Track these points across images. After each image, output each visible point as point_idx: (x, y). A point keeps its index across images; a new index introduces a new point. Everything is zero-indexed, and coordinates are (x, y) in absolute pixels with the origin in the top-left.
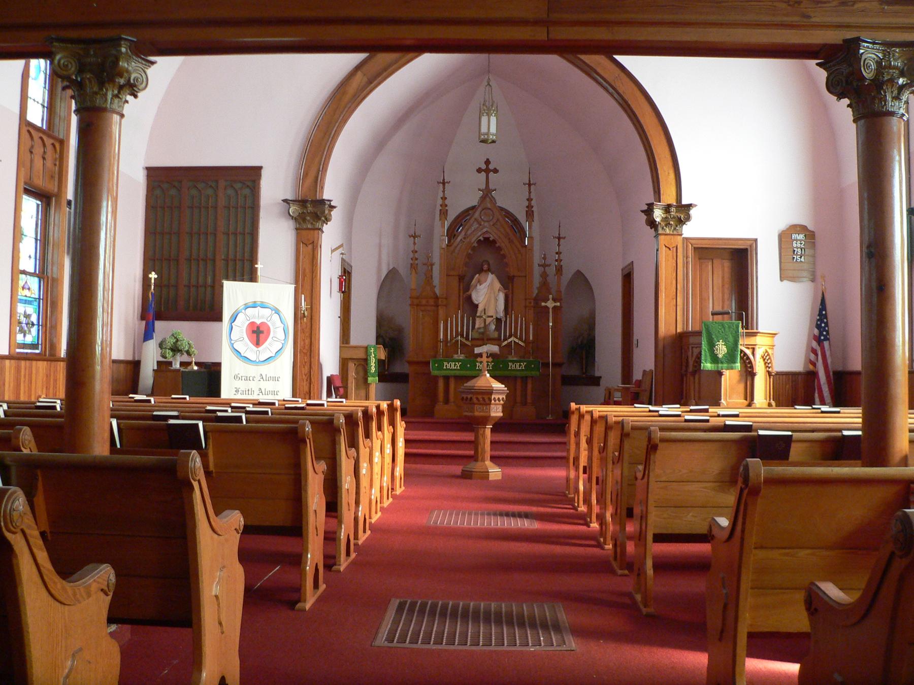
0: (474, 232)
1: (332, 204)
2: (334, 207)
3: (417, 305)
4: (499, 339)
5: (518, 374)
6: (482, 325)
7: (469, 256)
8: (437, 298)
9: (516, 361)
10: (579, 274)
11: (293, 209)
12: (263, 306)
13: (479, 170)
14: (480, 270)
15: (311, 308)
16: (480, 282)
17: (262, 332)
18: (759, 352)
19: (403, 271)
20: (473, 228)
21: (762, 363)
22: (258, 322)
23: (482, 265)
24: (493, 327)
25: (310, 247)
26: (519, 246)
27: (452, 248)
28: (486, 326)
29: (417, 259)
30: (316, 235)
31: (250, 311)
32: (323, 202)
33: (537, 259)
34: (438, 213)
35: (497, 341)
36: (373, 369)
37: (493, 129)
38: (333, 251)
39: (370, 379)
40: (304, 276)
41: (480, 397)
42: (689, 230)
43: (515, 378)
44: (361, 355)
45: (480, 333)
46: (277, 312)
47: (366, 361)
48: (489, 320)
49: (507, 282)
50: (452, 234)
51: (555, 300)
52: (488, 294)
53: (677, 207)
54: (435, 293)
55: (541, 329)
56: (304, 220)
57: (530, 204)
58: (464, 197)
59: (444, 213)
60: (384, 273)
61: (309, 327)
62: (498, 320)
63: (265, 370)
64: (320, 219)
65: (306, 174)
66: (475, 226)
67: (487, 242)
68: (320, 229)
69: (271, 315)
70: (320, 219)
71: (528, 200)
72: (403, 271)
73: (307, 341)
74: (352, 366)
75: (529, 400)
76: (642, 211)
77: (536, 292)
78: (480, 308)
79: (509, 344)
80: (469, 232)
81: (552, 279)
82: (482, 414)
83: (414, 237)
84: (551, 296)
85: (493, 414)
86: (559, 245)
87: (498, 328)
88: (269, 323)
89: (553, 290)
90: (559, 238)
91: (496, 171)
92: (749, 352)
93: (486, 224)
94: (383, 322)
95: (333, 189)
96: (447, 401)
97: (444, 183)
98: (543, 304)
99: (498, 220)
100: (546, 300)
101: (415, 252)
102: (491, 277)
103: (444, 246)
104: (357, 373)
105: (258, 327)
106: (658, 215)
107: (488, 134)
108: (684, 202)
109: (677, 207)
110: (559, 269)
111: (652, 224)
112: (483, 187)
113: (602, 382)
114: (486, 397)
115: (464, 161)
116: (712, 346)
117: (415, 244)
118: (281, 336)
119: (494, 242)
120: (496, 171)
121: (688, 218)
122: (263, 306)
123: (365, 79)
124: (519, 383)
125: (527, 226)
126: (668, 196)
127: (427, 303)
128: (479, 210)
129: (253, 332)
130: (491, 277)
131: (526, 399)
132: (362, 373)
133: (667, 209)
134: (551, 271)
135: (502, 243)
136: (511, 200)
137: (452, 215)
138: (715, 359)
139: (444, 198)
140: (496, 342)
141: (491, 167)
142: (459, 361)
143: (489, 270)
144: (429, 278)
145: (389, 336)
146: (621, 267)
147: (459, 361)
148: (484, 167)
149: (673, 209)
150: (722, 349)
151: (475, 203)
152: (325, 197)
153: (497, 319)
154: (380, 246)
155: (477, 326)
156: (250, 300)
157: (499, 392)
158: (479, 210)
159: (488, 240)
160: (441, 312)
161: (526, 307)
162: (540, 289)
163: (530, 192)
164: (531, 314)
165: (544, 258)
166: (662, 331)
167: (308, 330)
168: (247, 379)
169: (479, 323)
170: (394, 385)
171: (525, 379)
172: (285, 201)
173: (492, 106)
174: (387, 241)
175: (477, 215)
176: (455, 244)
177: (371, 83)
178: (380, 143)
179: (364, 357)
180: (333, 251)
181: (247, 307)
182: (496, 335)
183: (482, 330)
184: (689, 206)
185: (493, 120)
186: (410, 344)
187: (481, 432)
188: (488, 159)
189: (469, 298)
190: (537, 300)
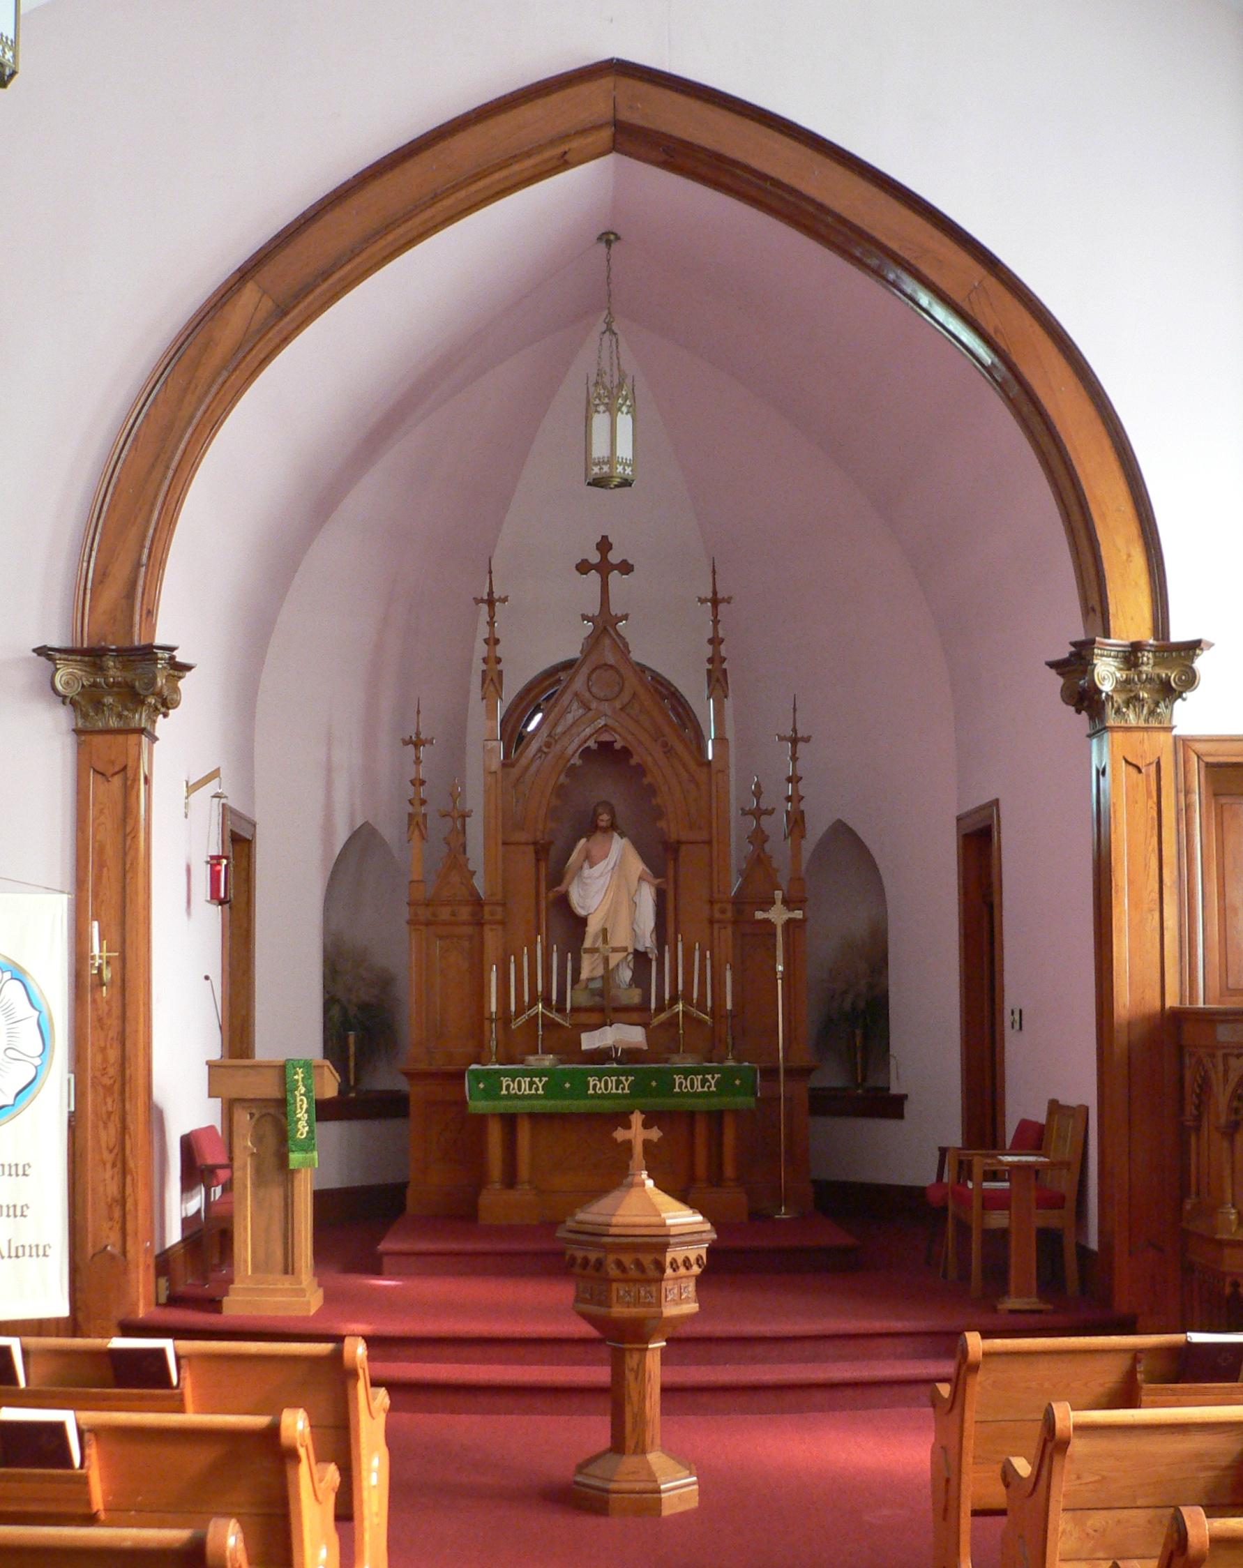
0: (572, 727)
1: (180, 657)
2: (188, 668)
3: (428, 924)
4: (643, 1007)
5: (701, 1104)
6: (600, 971)
7: (560, 791)
8: (478, 903)
9: (695, 1072)
10: (842, 833)
13: (583, 567)
14: (590, 827)
15: (123, 958)
16: (590, 859)
19: (390, 831)
20: (570, 718)
23: (595, 815)
24: (626, 975)
25: (117, 781)
26: (692, 766)
27: (515, 772)
28: (608, 975)
29: (423, 802)
30: (132, 751)
32: (148, 653)
33: (736, 796)
34: (476, 680)
35: (637, 1013)
37: (625, 449)
38: (192, 788)
39: (295, 1158)
40: (101, 865)
41: (627, 1259)
43: (691, 1115)
44: (270, 1090)
45: (594, 993)
47: (282, 1105)
48: (615, 959)
49: (662, 857)
50: (514, 736)
51: (788, 903)
52: (612, 891)
53: (1157, 650)
54: (473, 892)
55: (754, 985)
56: (98, 705)
57: (716, 651)
58: (546, 635)
59: (492, 680)
60: (342, 836)
61: (116, 1011)
62: (640, 958)
64: (142, 703)
65: (102, 576)
66: (576, 711)
67: (607, 754)
68: (142, 731)
70: (142, 703)
71: (711, 641)
72: (390, 831)
73: (113, 1054)
74: (243, 1118)
75: (729, 1171)
76: (1052, 665)
78: (593, 927)
79: (672, 1022)
80: (559, 730)
81: (779, 849)
82: (634, 1311)
83: (417, 743)
84: (778, 895)
85: (670, 1311)
86: (794, 758)
87: (640, 978)
89: (783, 879)
90: (795, 741)
91: (625, 568)
93: (605, 707)
94: (338, 963)
95: (189, 611)
96: (510, 1180)
97: (491, 602)
98: (759, 915)
99: (634, 695)
100: (768, 903)
101: (418, 782)
102: (619, 846)
103: (495, 765)
104: (258, 1140)
106: (1106, 673)
107: (611, 460)
108: (1178, 634)
109: (1157, 650)
110: (797, 822)
111: (1086, 700)
112: (594, 610)
113: (908, 1108)
114: (647, 1259)
115: (545, 531)
117: (418, 761)
118: (33, 1044)
119: (626, 752)
120: (625, 568)
121: (1190, 680)
123: (267, 304)
124: (701, 1128)
125: (707, 712)
126: (1130, 620)
127: (455, 915)
128: (585, 670)
130: (619, 846)
131: (720, 1166)
132: (271, 1141)
133: (1131, 656)
134: (776, 825)
135: (647, 753)
136: (667, 646)
137: (513, 685)
139: (493, 641)
140: (635, 1016)
141: (614, 557)
142: (540, 1073)
143: (613, 827)
145: (357, 1020)
146: (956, 813)
147: (540, 1073)
148: (595, 558)
149: (1147, 657)
151: (574, 652)
152: (159, 640)
153: (637, 953)
154: (329, 770)
155: (584, 975)
157: (688, 1238)
158: (585, 670)
159: (612, 749)
160: (492, 938)
161: (711, 922)
162: (747, 876)
163: (716, 622)
164: (726, 935)
165: (758, 794)
166: (1125, 1000)
167: (113, 1023)
169: (589, 967)
170: (377, 1127)
171: (716, 1117)
172: (42, 651)
173: (620, 386)
174: (347, 757)
175: (579, 683)
176: (524, 761)
177: (285, 313)
178: (319, 502)
179: (278, 1095)
180: (192, 788)
182: (635, 996)
183: (597, 985)
184: (1193, 647)
185: (624, 422)
186: (411, 1028)
187: (631, 1361)
188: (605, 538)
189: (563, 902)
190: (744, 904)
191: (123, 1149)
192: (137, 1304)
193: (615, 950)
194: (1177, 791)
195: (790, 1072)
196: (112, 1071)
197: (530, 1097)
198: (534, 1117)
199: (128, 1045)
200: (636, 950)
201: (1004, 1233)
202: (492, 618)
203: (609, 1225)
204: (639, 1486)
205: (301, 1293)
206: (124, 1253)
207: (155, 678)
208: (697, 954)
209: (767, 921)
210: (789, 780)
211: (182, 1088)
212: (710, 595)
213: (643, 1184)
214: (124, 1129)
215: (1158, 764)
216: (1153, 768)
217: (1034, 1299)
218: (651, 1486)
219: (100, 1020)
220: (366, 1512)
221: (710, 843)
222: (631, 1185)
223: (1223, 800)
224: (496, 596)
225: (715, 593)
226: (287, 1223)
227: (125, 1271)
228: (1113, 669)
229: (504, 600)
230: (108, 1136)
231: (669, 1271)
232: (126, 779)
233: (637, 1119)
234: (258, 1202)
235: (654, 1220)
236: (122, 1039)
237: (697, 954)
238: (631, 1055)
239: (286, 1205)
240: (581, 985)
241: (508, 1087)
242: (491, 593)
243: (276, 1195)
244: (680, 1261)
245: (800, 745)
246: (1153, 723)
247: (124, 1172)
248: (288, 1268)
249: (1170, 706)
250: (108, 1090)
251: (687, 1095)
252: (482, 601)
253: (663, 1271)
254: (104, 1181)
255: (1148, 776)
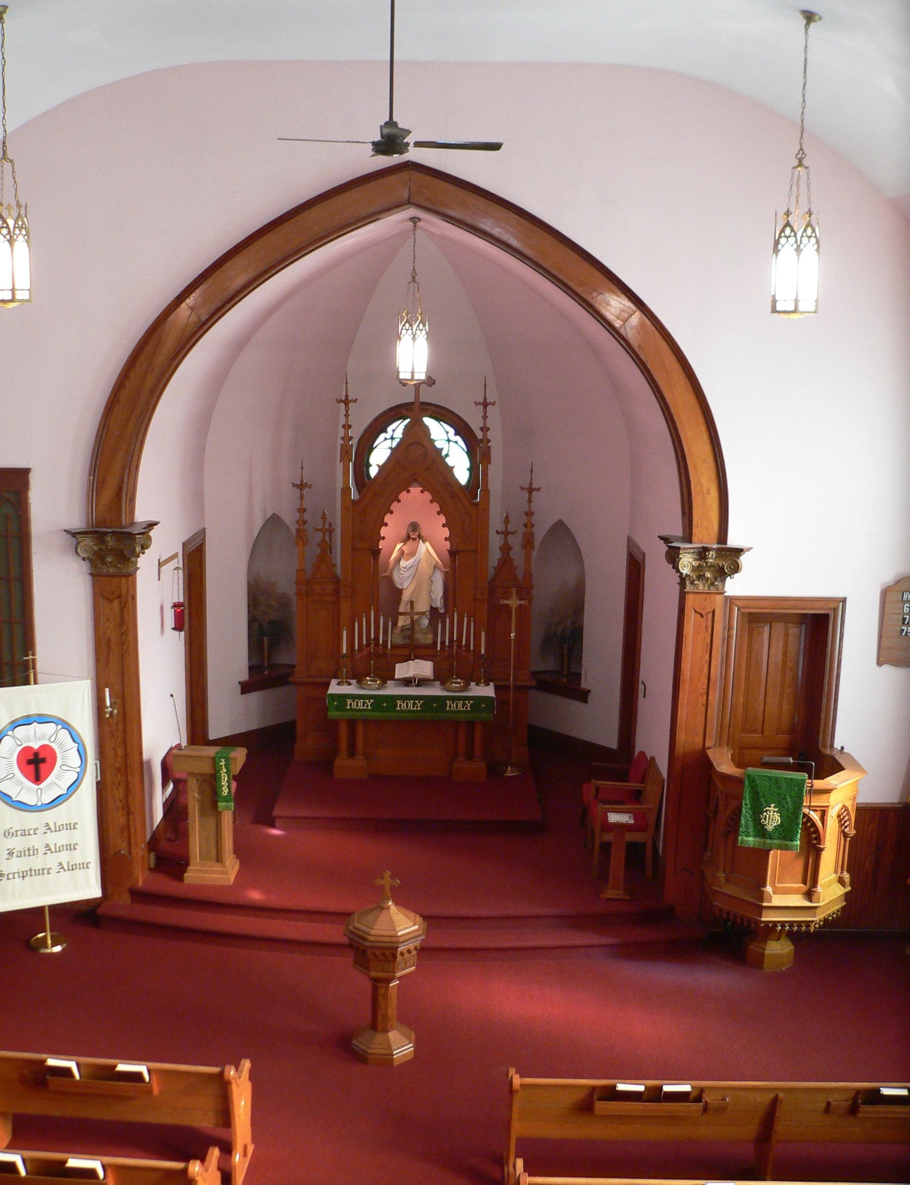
11: (88, 542)
12: (43, 719)
17: (43, 760)
18: (832, 813)
21: (837, 825)
22: (36, 746)
24: (425, 622)
25: (116, 603)
31: (20, 731)
33: (495, 522)
36: (226, 787)
38: (160, 565)
39: (221, 805)
42: (734, 586)
43: (457, 723)
46: (66, 725)
63: (50, 816)
69: (56, 732)
73: (120, 752)
75: (478, 752)
77: (491, 572)
78: (406, 596)
88: (52, 745)
92: (815, 816)
94: (258, 596)
104: (201, 792)
105: (36, 754)
108: (733, 541)
116: (757, 811)
117: (302, 497)
118: (75, 761)
121: (736, 569)
122: (43, 719)
126: (705, 533)
129: (30, 762)
133: (702, 553)
134: (516, 541)
138: (761, 831)
144: (326, 548)
149: (712, 554)
150: (773, 818)
155: (400, 624)
156: (19, 714)
160: (345, 608)
163: (485, 417)
168: (25, 833)
181: (15, 724)
182: (428, 639)
184: (739, 551)
191: (127, 802)
192: (138, 879)
193: (418, 613)
194: (724, 628)
195: (515, 687)
196: (120, 760)
197: (362, 710)
198: (366, 721)
199: (128, 746)
200: (431, 607)
201: (609, 844)
202: (347, 412)
203: (368, 934)
204: (382, 1052)
205: (226, 873)
206: (130, 853)
207: (135, 548)
208: (466, 619)
209: (507, 605)
210: (527, 514)
211: (161, 728)
212: (482, 401)
213: (389, 908)
214: (128, 791)
215: (714, 612)
216: (711, 614)
217: (622, 892)
218: (388, 1052)
219: (112, 733)
220: (237, 1123)
221: (476, 551)
222: (382, 908)
223: (753, 625)
224: (350, 398)
225: (485, 399)
226: (217, 834)
227: (131, 863)
228: (691, 560)
229: (355, 401)
230: (119, 794)
231: (399, 957)
232: (121, 603)
233: (388, 873)
234: (202, 826)
235: (392, 933)
236: (125, 743)
237: (466, 619)
238: (422, 682)
239: (217, 827)
240: (397, 631)
241: (351, 705)
242: (347, 396)
243: (212, 821)
244: (405, 951)
245: (534, 493)
246: (713, 589)
247: (129, 813)
248: (219, 859)
249: (723, 581)
250: (119, 770)
251: (455, 712)
252: (341, 401)
253: (396, 958)
254: (117, 818)
255: (707, 619)
